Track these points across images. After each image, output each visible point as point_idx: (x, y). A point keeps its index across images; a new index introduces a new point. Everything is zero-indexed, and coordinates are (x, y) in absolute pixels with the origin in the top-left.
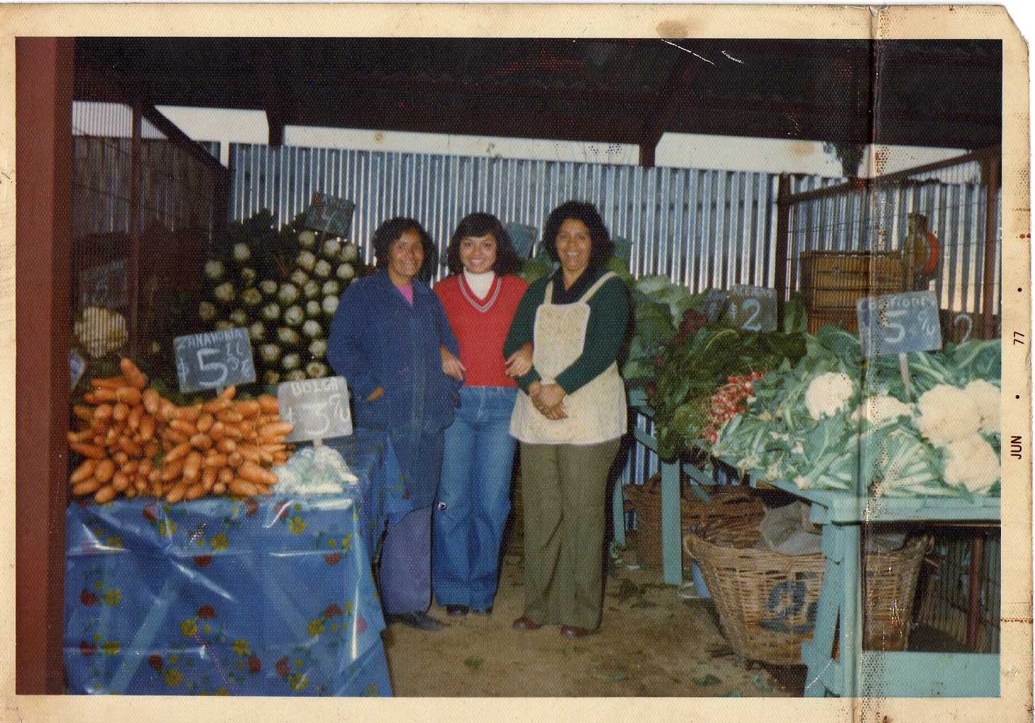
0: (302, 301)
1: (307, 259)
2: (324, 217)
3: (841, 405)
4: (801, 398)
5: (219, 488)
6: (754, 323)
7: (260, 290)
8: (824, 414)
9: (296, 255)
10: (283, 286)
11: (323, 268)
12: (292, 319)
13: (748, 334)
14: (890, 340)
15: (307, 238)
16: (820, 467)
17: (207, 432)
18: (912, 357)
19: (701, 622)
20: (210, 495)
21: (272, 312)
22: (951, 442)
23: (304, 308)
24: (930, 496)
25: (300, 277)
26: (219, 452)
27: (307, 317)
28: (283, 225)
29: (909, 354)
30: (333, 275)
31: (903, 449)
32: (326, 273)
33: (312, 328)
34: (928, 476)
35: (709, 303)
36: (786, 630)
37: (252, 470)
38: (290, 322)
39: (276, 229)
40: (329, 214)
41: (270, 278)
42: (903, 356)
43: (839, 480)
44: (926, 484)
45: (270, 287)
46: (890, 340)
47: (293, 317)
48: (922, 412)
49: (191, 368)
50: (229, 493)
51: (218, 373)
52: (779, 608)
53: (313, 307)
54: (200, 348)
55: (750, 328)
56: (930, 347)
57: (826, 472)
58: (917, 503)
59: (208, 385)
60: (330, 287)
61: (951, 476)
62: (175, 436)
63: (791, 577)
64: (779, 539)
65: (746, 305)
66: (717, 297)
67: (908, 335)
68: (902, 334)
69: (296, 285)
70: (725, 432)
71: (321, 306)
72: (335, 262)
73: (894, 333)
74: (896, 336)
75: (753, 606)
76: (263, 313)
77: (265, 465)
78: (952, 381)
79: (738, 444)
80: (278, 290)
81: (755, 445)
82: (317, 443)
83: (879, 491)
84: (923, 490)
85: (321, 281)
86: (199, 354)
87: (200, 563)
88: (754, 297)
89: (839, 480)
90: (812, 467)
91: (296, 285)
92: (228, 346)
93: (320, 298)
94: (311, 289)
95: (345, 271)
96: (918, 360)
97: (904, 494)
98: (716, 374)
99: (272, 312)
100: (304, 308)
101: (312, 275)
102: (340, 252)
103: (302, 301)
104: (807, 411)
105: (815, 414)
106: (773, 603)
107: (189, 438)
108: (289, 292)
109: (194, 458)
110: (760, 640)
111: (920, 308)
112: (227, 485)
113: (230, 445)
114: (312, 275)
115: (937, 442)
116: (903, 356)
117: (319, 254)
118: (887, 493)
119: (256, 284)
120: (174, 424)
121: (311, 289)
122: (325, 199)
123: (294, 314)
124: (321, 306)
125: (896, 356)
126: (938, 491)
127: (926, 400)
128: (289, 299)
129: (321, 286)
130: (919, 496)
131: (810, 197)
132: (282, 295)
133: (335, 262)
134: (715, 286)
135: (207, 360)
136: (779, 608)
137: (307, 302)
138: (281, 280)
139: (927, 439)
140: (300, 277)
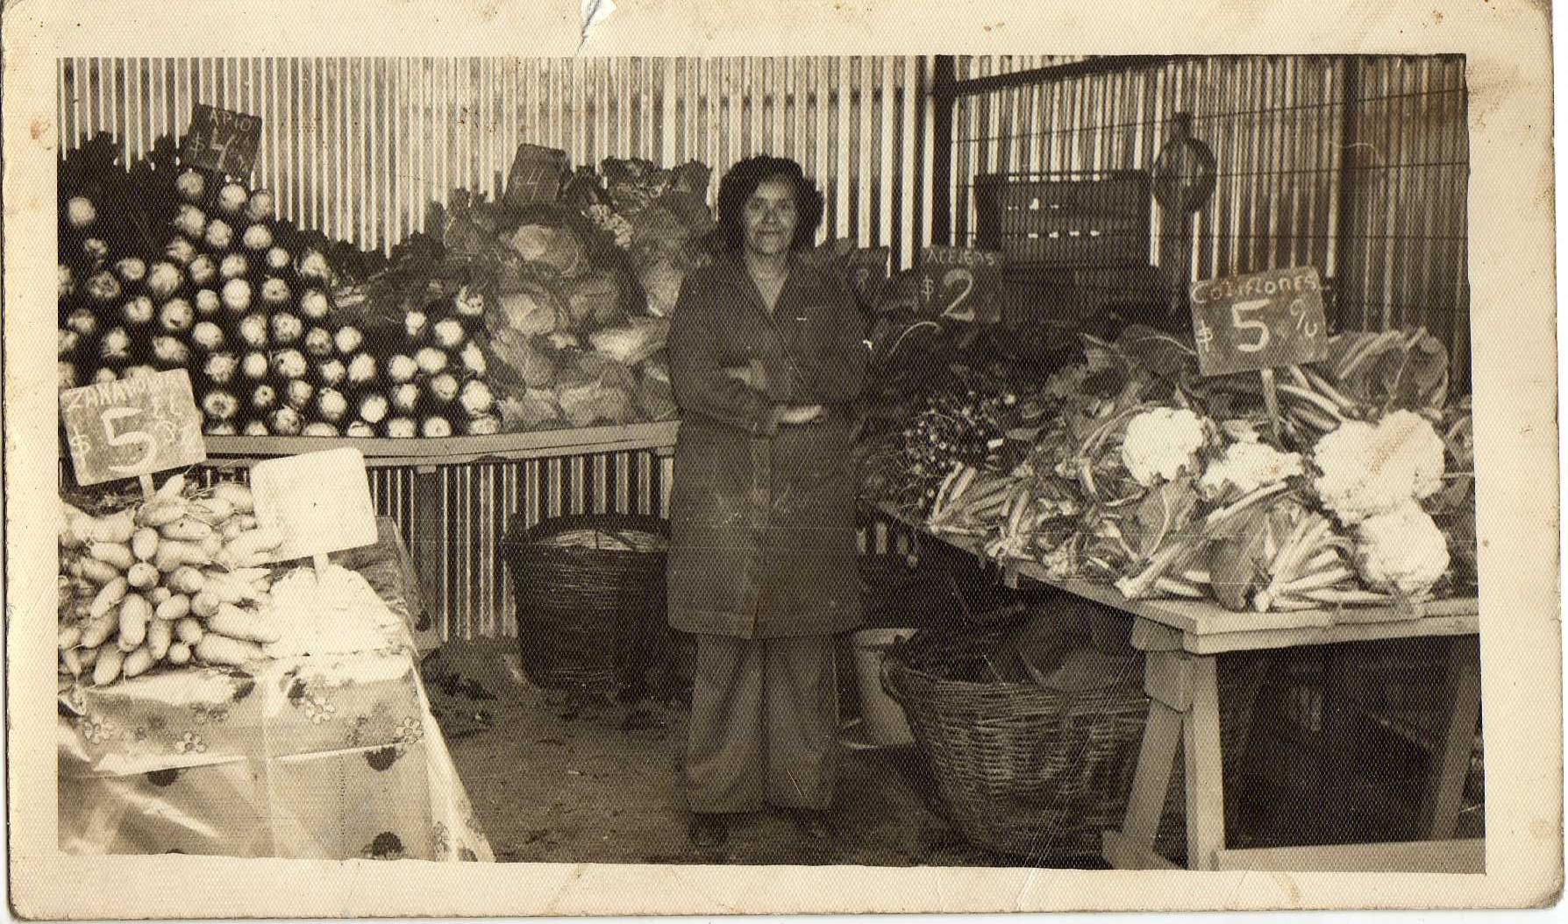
0: (188, 290)
1: (192, 219)
2: (215, 147)
3: (1186, 461)
4: (1109, 447)
5: (180, 654)
6: (962, 308)
7: (118, 275)
8: (1159, 475)
9: (175, 212)
10: (155, 267)
11: (220, 233)
12: (173, 322)
13: (960, 327)
14: (1246, 348)
15: (191, 183)
16: (1160, 561)
17: (152, 561)
18: (1281, 375)
19: (897, 793)
20: (163, 666)
21: (140, 310)
22: (1368, 517)
23: (193, 303)
24: (1348, 605)
25: (182, 249)
26: (175, 591)
27: (199, 317)
28: (134, 157)
29: (1275, 369)
30: (236, 245)
31: (1300, 530)
32: (226, 242)
33: (208, 334)
34: (1341, 573)
35: (855, 267)
36: (1059, 806)
37: (229, 619)
38: (170, 326)
39: (122, 166)
40: (221, 141)
41: (131, 255)
42: (1267, 374)
43: (1187, 582)
44: (1338, 586)
45: (133, 268)
46: (1246, 348)
47: (176, 318)
48: (1324, 469)
49: (95, 442)
50: (196, 661)
51: (140, 448)
52: (1047, 772)
53: (206, 300)
54: (106, 407)
55: (957, 316)
56: (1310, 357)
57: (1167, 573)
58: (1323, 618)
59: (125, 471)
60: (233, 265)
61: (1374, 571)
62: (97, 570)
63: (1067, 724)
64: (1049, 666)
65: (949, 279)
66: (865, 259)
67: (1274, 338)
68: (1265, 338)
69: (177, 264)
70: (947, 495)
71: (220, 296)
72: (239, 221)
73: (1252, 336)
74: (1256, 342)
75: (1004, 772)
76: (124, 314)
77: (245, 604)
78: (1356, 413)
79: (992, 516)
80: (148, 273)
81: (1015, 520)
82: (321, 560)
83: (1262, 600)
84: (1329, 596)
85: (216, 256)
86: (106, 418)
87: (162, 780)
88: (963, 266)
89: (1187, 582)
90: (1145, 564)
91: (177, 264)
92: (155, 400)
93: (217, 284)
94: (201, 269)
95: (257, 236)
96: (1291, 379)
97: (1291, 599)
98: (908, 396)
99: (140, 310)
100: (193, 303)
101: (201, 245)
102: (244, 206)
103: (188, 290)
104: (1123, 471)
105: (1142, 474)
106: (1036, 764)
107: (123, 572)
108: (166, 276)
109: (135, 605)
110: (1012, 821)
111: (1293, 294)
112: (192, 648)
113: (192, 579)
114: (201, 245)
115: (1346, 518)
116: (1267, 374)
117: (211, 207)
118: (1281, 602)
119: (110, 264)
120: (97, 550)
121: (201, 269)
122: (214, 115)
123: (176, 312)
124: (220, 296)
125: (1258, 374)
126: (1356, 595)
127: (1327, 450)
128: (168, 288)
129: (218, 264)
130: (1326, 606)
131: (987, 85)
132: (155, 281)
133: (239, 221)
134: (839, 236)
135: (121, 427)
136: (1047, 772)
137: (196, 293)
138: (154, 255)
139: (1332, 512)
140: (182, 249)
